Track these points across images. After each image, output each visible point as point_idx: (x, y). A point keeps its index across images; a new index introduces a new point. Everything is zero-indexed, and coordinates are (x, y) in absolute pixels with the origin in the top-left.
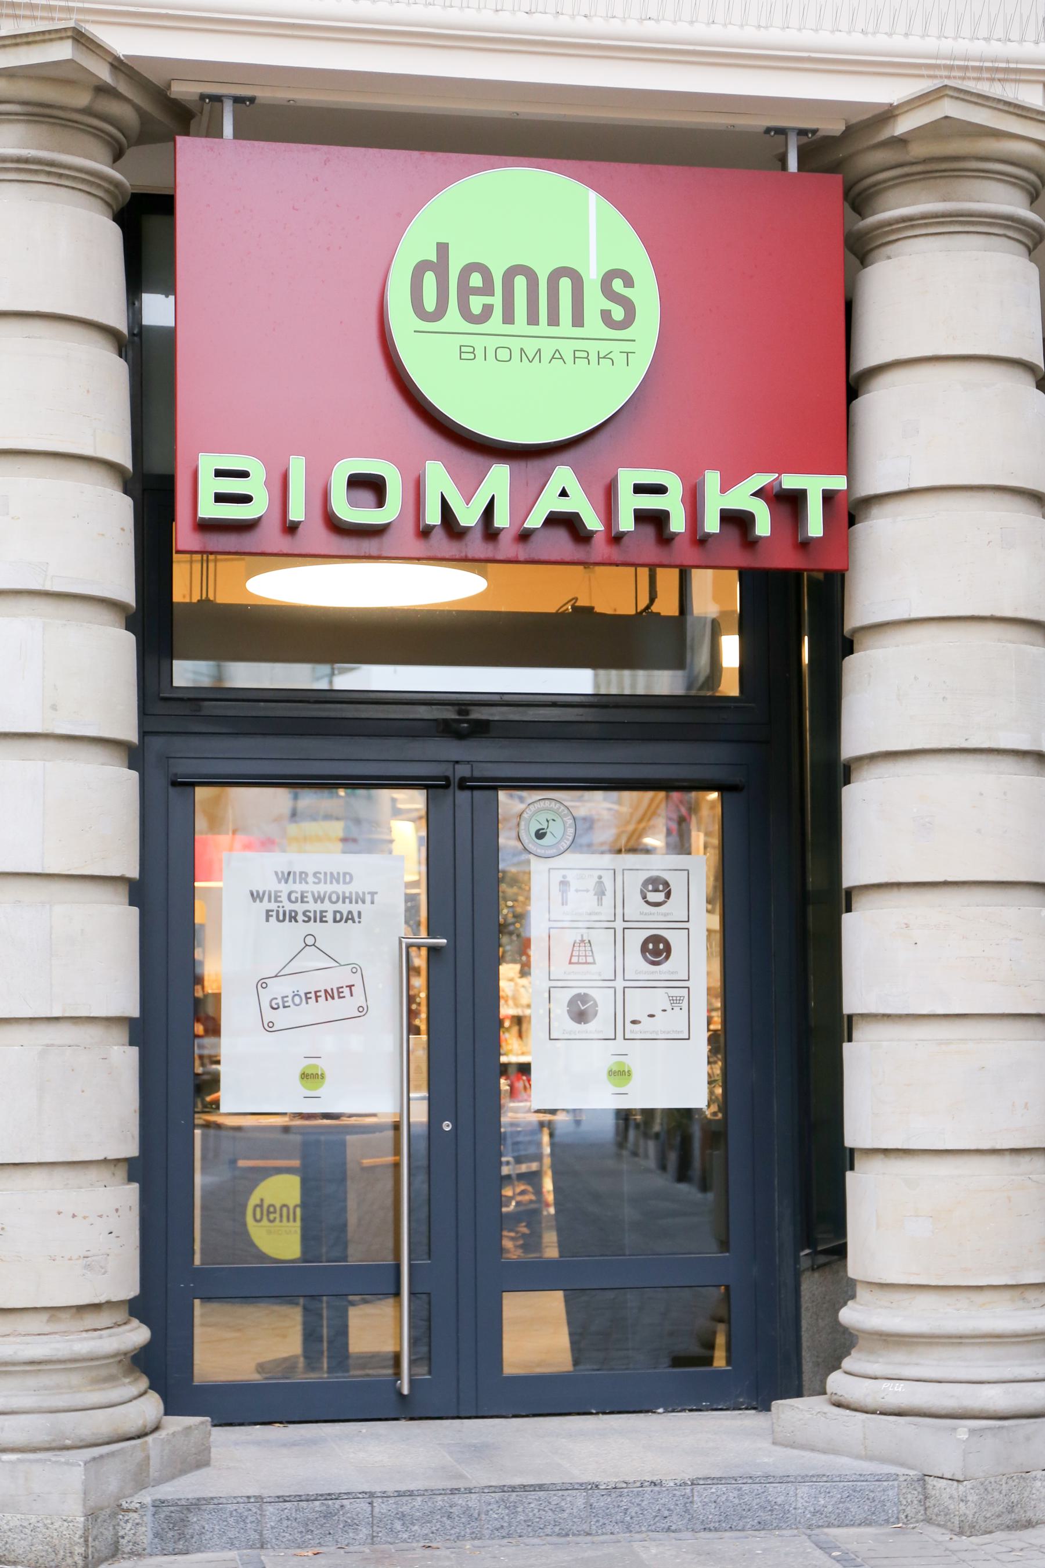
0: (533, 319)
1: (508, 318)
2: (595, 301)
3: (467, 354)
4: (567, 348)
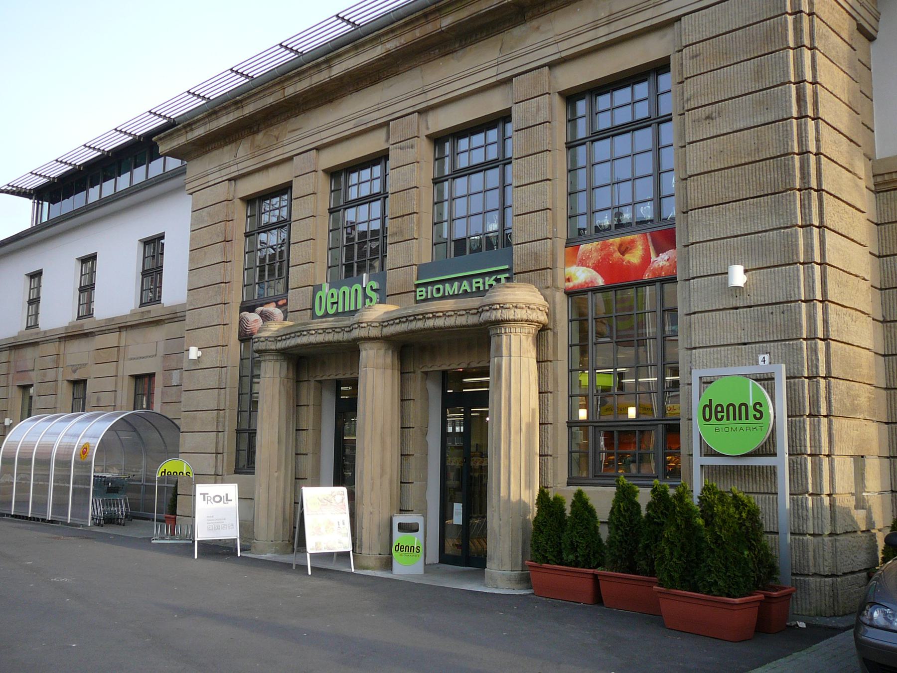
0: (735, 419)
1: (728, 419)
2: (751, 412)
3: (717, 430)
4: (744, 426)
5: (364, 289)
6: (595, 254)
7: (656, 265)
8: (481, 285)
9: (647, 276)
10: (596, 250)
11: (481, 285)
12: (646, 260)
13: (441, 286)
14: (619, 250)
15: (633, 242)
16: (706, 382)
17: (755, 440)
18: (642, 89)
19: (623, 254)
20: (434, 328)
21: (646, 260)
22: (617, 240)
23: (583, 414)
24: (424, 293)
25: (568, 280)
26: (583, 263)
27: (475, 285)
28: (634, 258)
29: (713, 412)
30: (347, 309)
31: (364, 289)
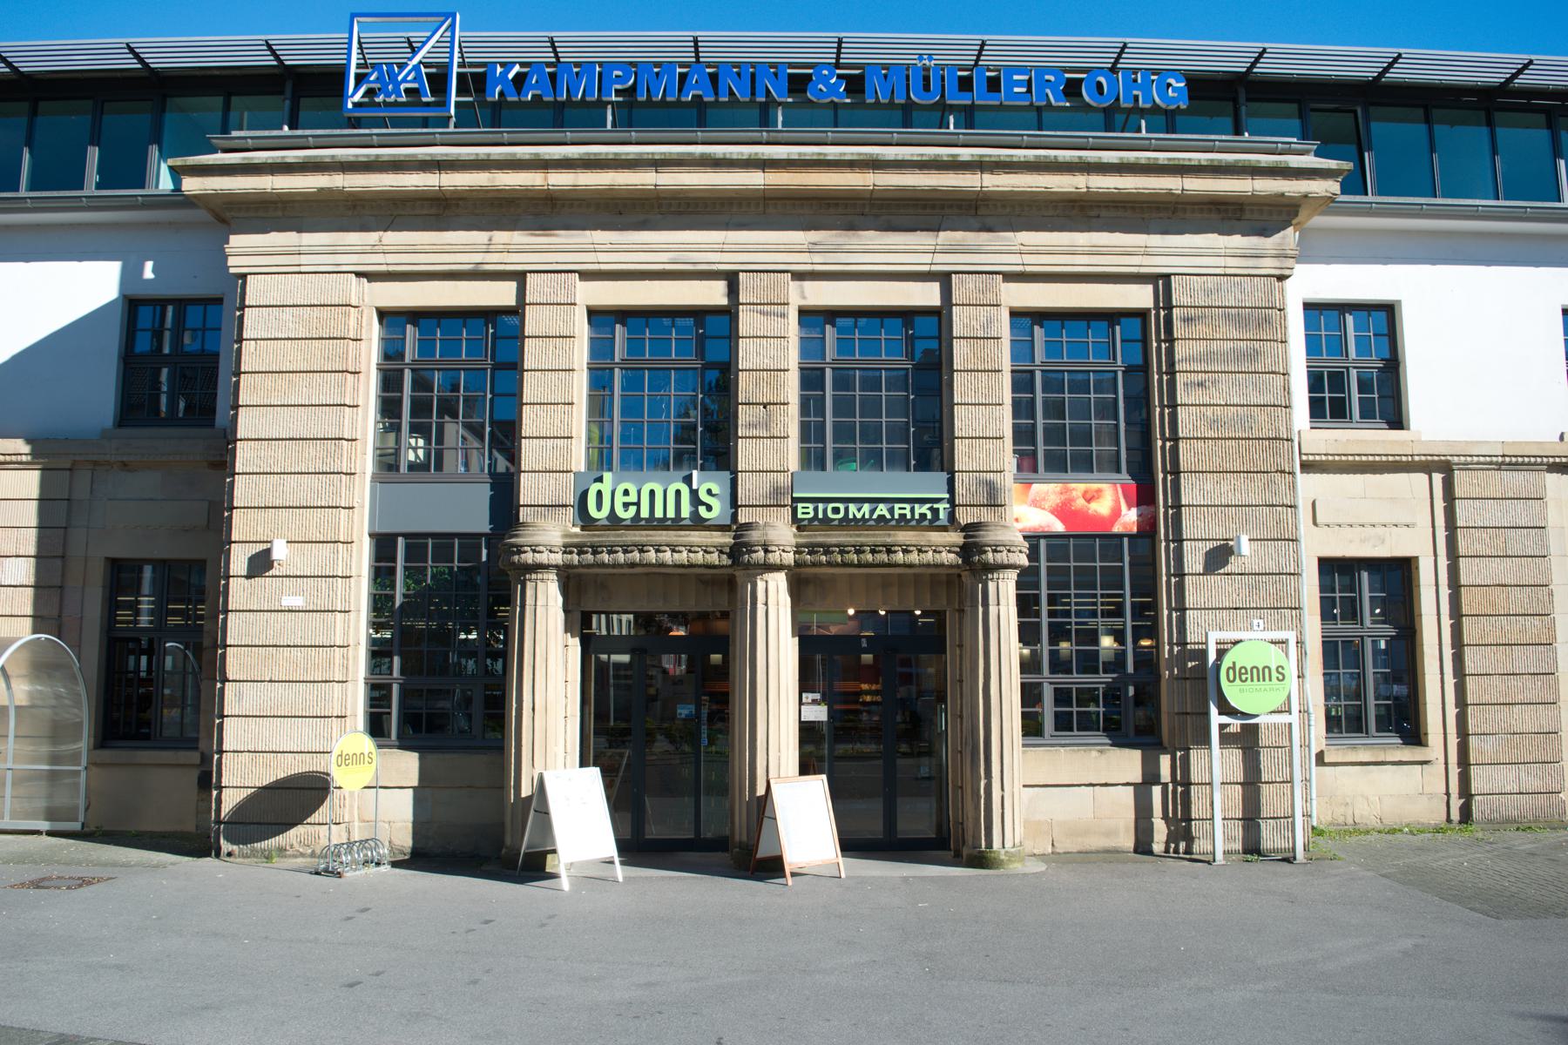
3: (1241, 691)
5: (694, 494)
8: (907, 512)
11: (907, 512)
12: (1116, 513)
13: (841, 506)
14: (1084, 496)
15: (1099, 491)
17: (1277, 701)
19: (1089, 501)
21: (1116, 513)
22: (1082, 487)
23: (716, 658)
24: (811, 510)
26: (1036, 503)
28: (1102, 507)
29: (1239, 674)
30: (659, 514)
31: (694, 494)
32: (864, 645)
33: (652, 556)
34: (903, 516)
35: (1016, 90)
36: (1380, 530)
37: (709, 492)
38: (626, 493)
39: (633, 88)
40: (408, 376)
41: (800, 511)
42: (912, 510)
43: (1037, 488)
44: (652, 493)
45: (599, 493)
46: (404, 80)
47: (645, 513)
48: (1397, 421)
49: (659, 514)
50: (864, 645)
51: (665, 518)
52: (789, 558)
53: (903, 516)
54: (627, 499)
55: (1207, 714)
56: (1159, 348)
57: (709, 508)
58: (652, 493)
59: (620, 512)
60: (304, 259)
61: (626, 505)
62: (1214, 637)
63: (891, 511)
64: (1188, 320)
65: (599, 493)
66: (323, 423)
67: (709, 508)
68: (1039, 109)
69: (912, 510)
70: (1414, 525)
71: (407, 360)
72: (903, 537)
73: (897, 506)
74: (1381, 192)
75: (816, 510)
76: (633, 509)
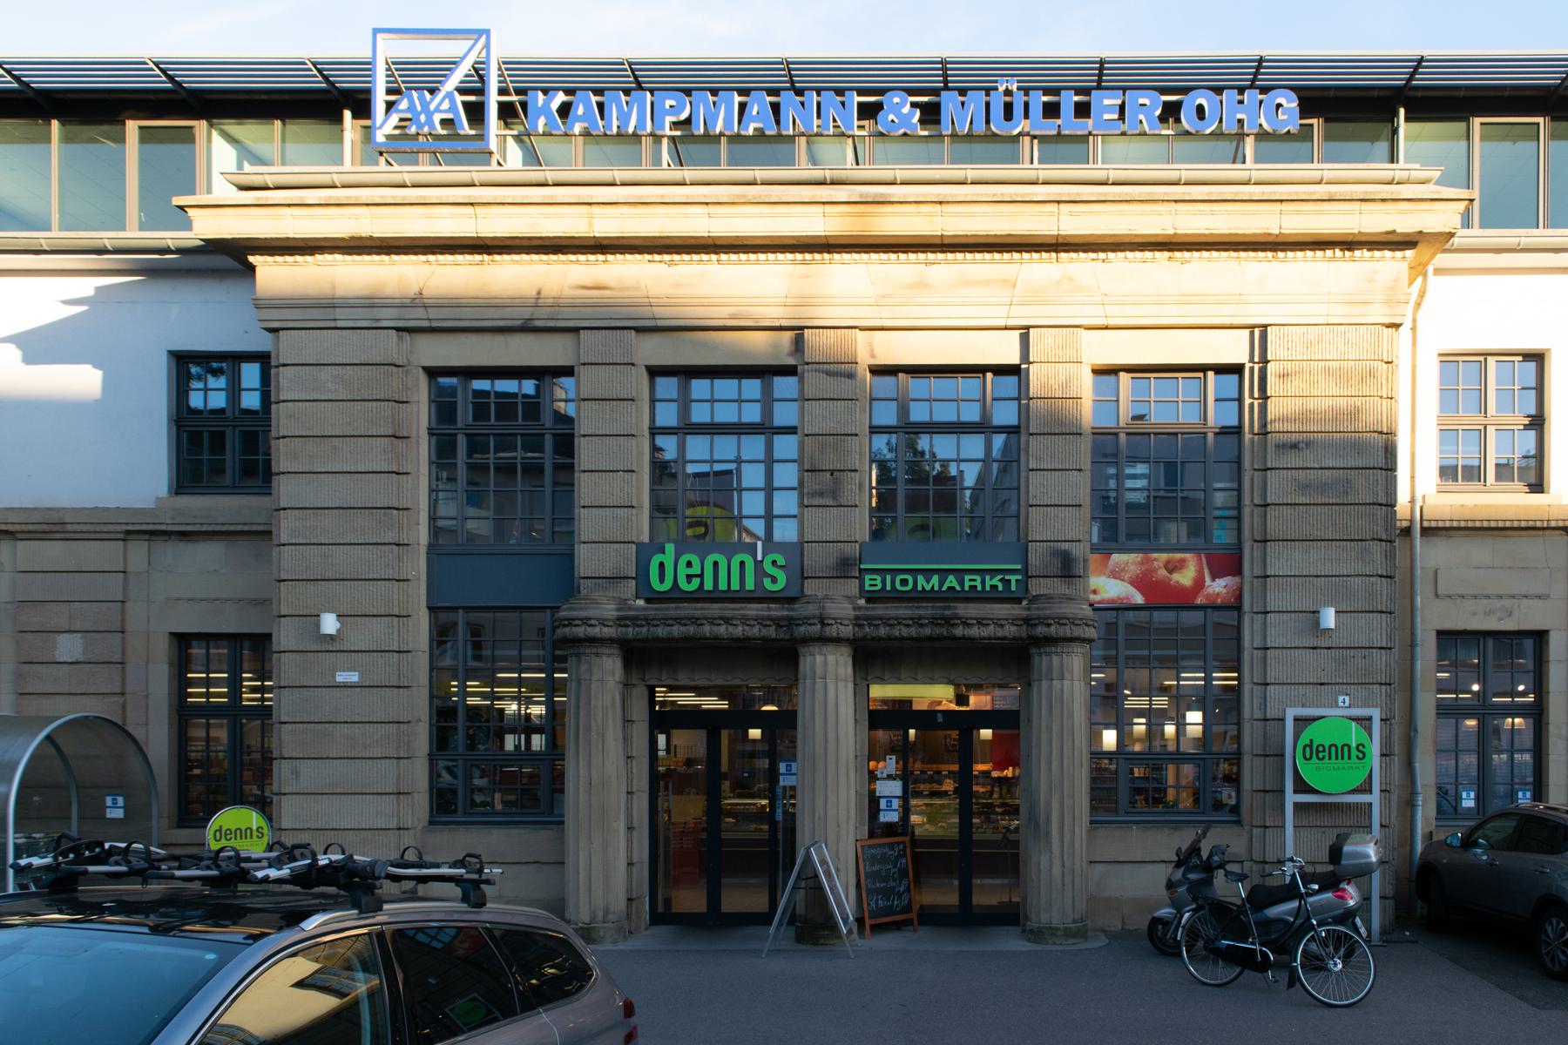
2: (1354, 753)
3: (1318, 769)
5: (758, 564)
6: (1132, 567)
7: (1210, 590)
8: (978, 584)
9: (1199, 601)
10: (1135, 563)
11: (978, 584)
12: (1199, 584)
14: (1166, 567)
15: (1183, 561)
16: (1302, 722)
17: (1358, 779)
18: (752, 387)
19: (1171, 572)
20: (669, 640)
21: (1199, 584)
22: (1164, 556)
24: (878, 582)
25: (1095, 592)
26: (1115, 575)
27: (967, 584)
28: (1185, 578)
29: (1315, 751)
30: (723, 586)
31: (758, 564)
32: (940, 720)
33: (707, 629)
34: (973, 588)
35: (1106, 117)
36: (1508, 603)
37: (774, 562)
38: (689, 564)
39: (688, 121)
40: (462, 442)
41: (867, 583)
42: (983, 583)
43: (1116, 557)
44: (716, 564)
45: (662, 565)
46: (437, 110)
47: (708, 586)
48: (1538, 486)
49: (723, 586)
50: (940, 720)
51: (1204, 679)
52: (847, 631)
53: (973, 588)
54: (690, 571)
55: (1282, 791)
56: (1252, 405)
57: (774, 580)
58: (716, 564)
59: (683, 585)
60: (339, 313)
61: (689, 577)
62: (1291, 713)
63: (962, 583)
64: (1284, 376)
65: (662, 565)
66: (377, 491)
67: (774, 580)
68: (640, 87)
69: (983, 583)
70: (1547, 597)
71: (460, 424)
72: (963, 610)
73: (967, 578)
74: (1481, 227)
75: (884, 582)
76: (696, 582)
